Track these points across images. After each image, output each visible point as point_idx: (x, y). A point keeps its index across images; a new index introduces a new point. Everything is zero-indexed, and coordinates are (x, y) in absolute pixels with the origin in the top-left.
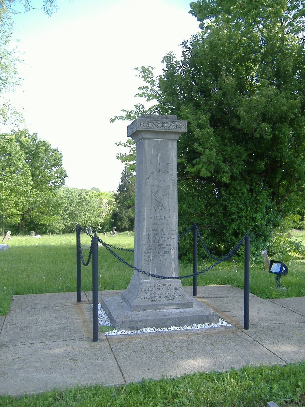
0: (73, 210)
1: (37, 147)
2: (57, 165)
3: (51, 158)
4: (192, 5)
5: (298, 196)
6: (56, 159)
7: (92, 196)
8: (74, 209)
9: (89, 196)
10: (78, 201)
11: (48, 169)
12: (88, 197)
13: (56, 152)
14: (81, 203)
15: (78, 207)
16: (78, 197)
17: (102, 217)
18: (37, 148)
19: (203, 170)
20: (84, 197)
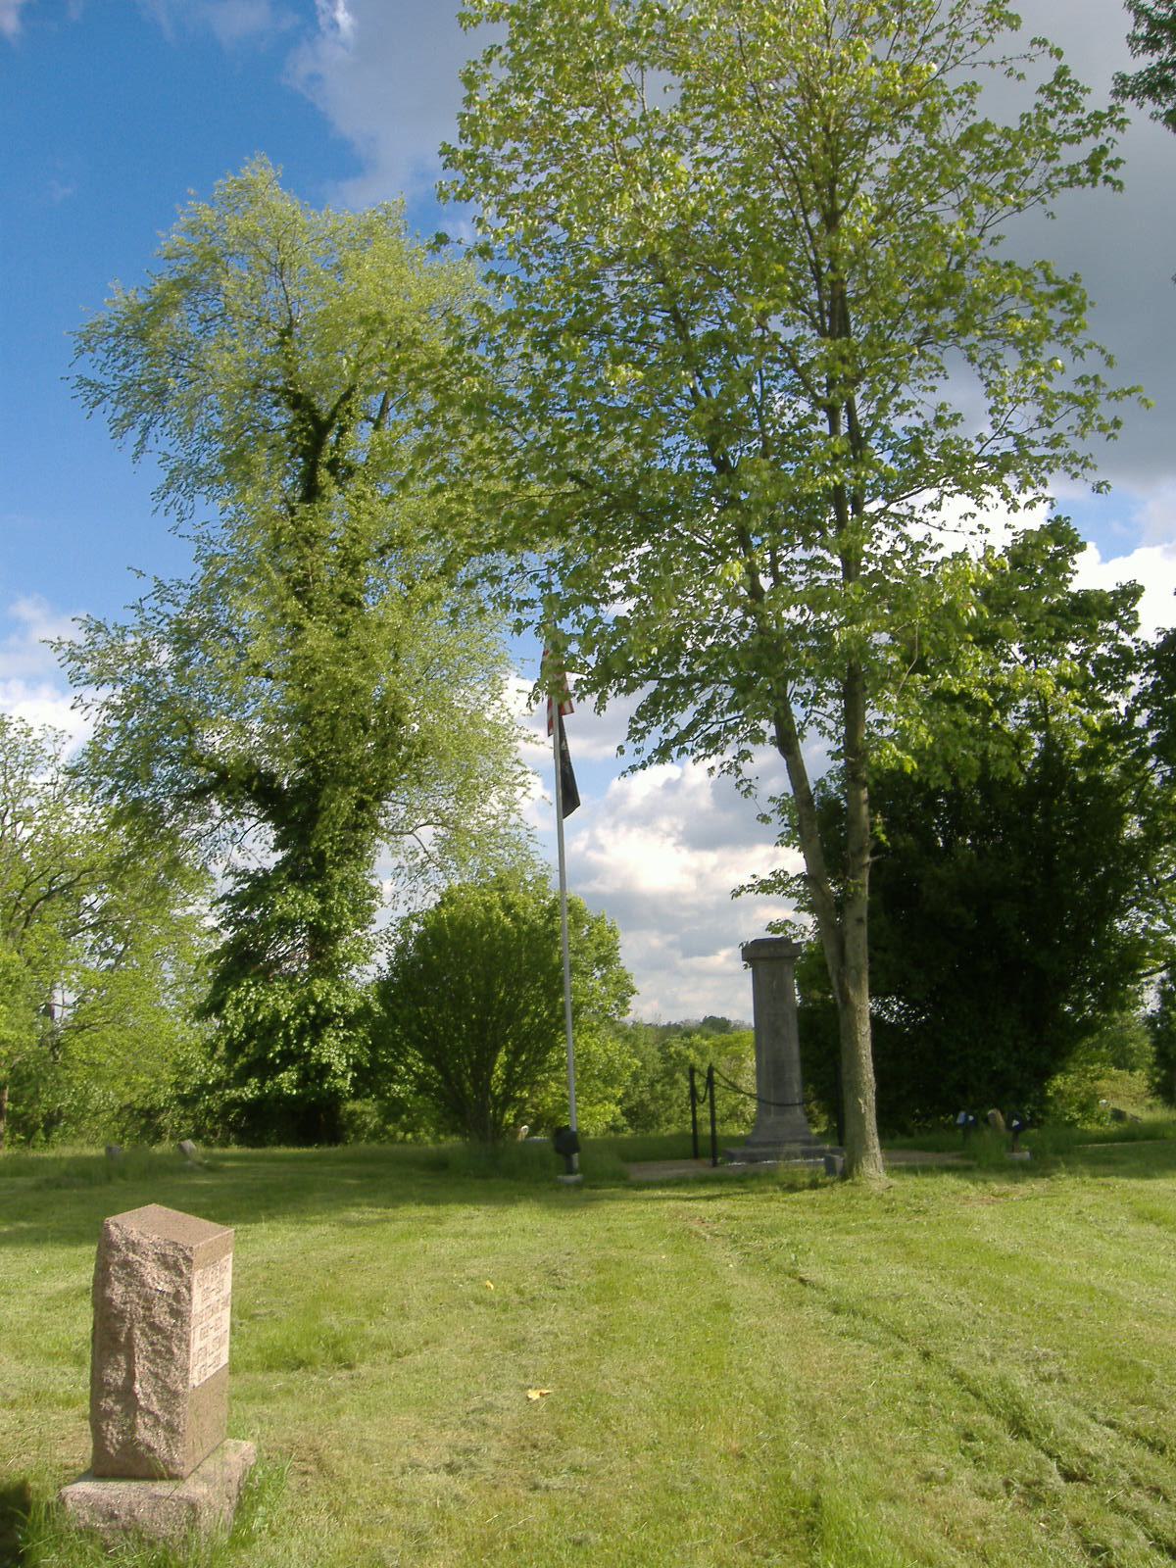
0: (642, 1101)
1: (552, 913)
2: (605, 961)
3: (589, 944)
4: (1142, 588)
5: (820, 433)
6: (601, 944)
7: (706, 1048)
8: (646, 1096)
9: (697, 1049)
10: (660, 1067)
11: (583, 973)
12: (691, 1053)
13: (599, 925)
14: (669, 1073)
15: (659, 1087)
16: (659, 1054)
17: (745, 1120)
18: (551, 919)
19: (487, 440)
20: (679, 1054)
